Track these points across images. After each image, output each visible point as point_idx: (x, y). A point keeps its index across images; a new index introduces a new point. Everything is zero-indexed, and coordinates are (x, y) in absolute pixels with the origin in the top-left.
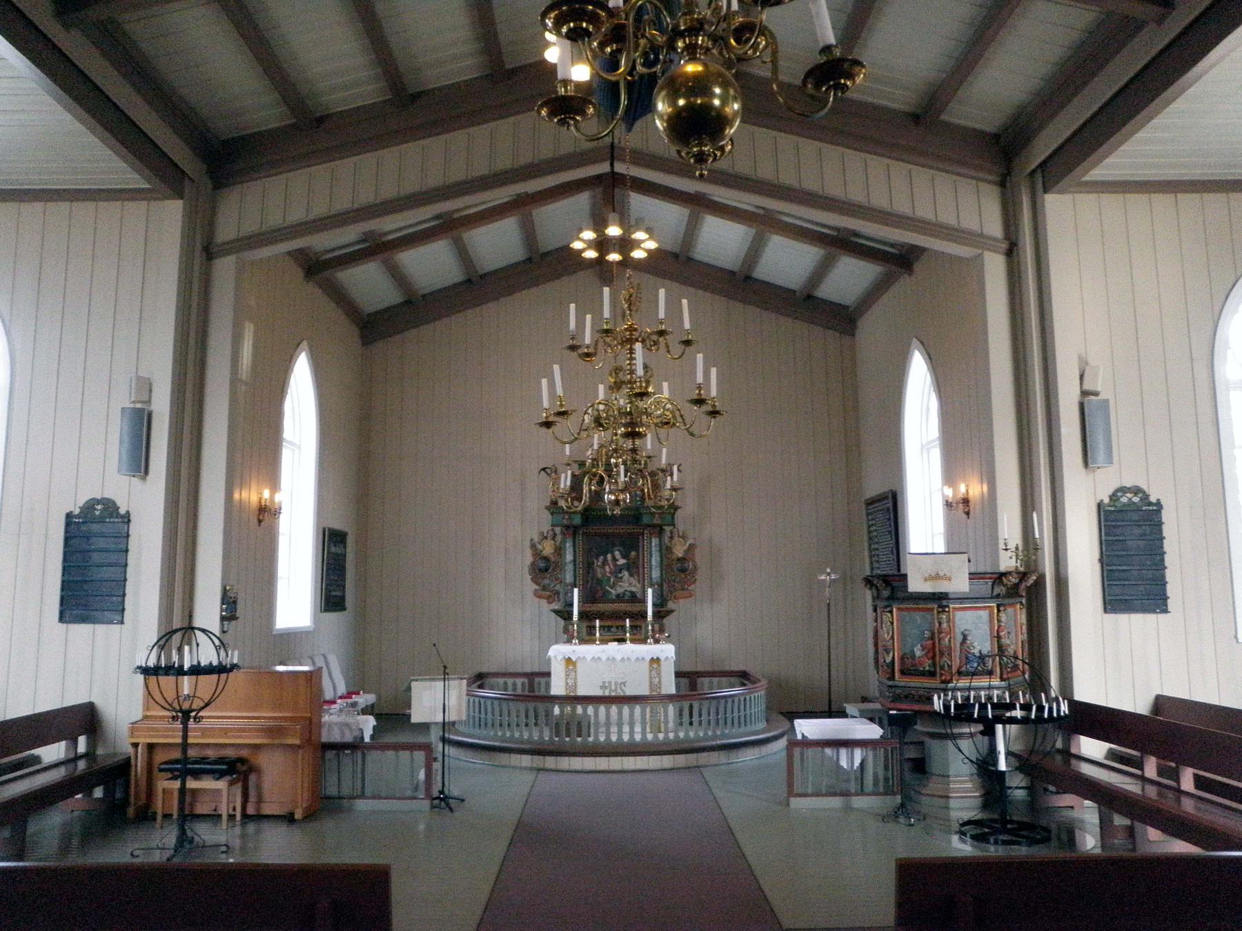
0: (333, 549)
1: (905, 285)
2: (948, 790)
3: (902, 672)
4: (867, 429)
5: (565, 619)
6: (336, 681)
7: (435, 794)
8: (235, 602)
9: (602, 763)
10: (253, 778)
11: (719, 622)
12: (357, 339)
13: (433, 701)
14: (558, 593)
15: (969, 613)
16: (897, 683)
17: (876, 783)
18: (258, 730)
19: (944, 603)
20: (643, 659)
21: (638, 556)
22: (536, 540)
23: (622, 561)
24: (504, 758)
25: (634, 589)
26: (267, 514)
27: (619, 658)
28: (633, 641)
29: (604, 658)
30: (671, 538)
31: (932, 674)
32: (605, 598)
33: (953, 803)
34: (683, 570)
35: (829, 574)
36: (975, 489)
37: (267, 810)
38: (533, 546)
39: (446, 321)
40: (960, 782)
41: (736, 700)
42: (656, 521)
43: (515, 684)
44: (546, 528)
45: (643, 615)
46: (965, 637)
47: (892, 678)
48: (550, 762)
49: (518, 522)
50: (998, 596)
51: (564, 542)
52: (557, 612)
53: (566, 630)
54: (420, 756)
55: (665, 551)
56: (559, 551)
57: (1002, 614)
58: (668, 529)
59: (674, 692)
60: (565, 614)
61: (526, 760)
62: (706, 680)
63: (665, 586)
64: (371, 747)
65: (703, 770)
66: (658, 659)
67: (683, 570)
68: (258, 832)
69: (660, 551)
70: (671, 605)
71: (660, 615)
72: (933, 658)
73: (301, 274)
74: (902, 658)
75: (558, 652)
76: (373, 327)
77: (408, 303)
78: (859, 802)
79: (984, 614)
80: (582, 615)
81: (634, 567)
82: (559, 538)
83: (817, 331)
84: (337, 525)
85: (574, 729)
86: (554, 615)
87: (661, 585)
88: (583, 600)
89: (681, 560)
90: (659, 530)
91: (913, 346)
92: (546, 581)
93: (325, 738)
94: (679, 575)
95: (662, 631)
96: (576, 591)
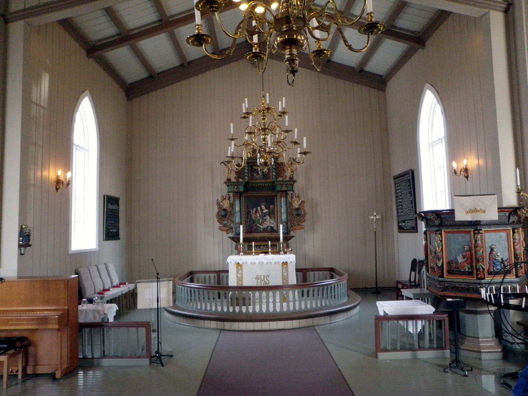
0: (110, 207)
1: (420, 55)
2: (479, 347)
3: (449, 272)
4: (395, 137)
5: (236, 242)
6: (113, 278)
7: (153, 354)
8: (28, 236)
9: (258, 326)
10: (31, 349)
11: (318, 242)
12: (125, 99)
13: (152, 295)
14: (232, 228)
15: (493, 234)
16: (445, 279)
17: (431, 341)
18: (33, 320)
19: (479, 228)
20: (278, 262)
21: (274, 208)
22: (220, 200)
23: (265, 211)
24: (201, 323)
25: (272, 225)
26: (62, 186)
27: (265, 262)
28: (273, 253)
29: (257, 263)
30: (292, 198)
31: (470, 274)
32: (257, 230)
33: (484, 356)
34: (298, 215)
35: (375, 216)
36: (471, 162)
37: (41, 370)
38: (218, 204)
39: (170, 87)
40: (486, 342)
41: (329, 287)
42: (284, 189)
43: (210, 277)
44: (225, 193)
45: (278, 239)
46: (492, 249)
47: (442, 276)
48: (227, 325)
49: (211, 189)
50: (513, 223)
51: (234, 201)
52: (232, 238)
53: (237, 248)
54: (143, 331)
55: (289, 205)
56: (232, 205)
57: (516, 235)
58: (290, 193)
59: (295, 283)
60: (236, 239)
61: (213, 324)
62: (312, 273)
63: (289, 223)
64: (113, 326)
65: (316, 328)
66: (286, 263)
67: (298, 215)
68: (34, 387)
69: (286, 204)
70: (292, 233)
71: (287, 238)
72: (471, 263)
73: (84, 53)
74: (449, 263)
75: (233, 259)
76: (132, 91)
77: (151, 77)
78: (422, 355)
79: (504, 235)
80: (245, 240)
81: (272, 214)
82: (232, 199)
83: (366, 89)
84: (113, 193)
85: (241, 301)
86: (230, 240)
87: (287, 223)
88: (245, 232)
89: (297, 209)
90: (285, 193)
91: (425, 87)
92: (225, 222)
93: (81, 320)
94: (296, 217)
95: (288, 247)
96: (241, 226)
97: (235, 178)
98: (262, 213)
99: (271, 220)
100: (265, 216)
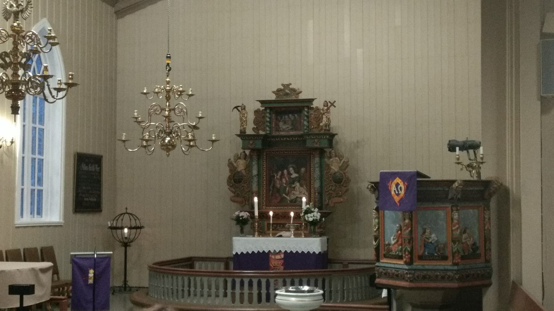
22: (232, 160)
23: (294, 175)
38: (230, 164)
56: (248, 168)
90: (321, 152)
97: (253, 129)
98: (290, 178)
99: (302, 188)
100: (293, 183)
